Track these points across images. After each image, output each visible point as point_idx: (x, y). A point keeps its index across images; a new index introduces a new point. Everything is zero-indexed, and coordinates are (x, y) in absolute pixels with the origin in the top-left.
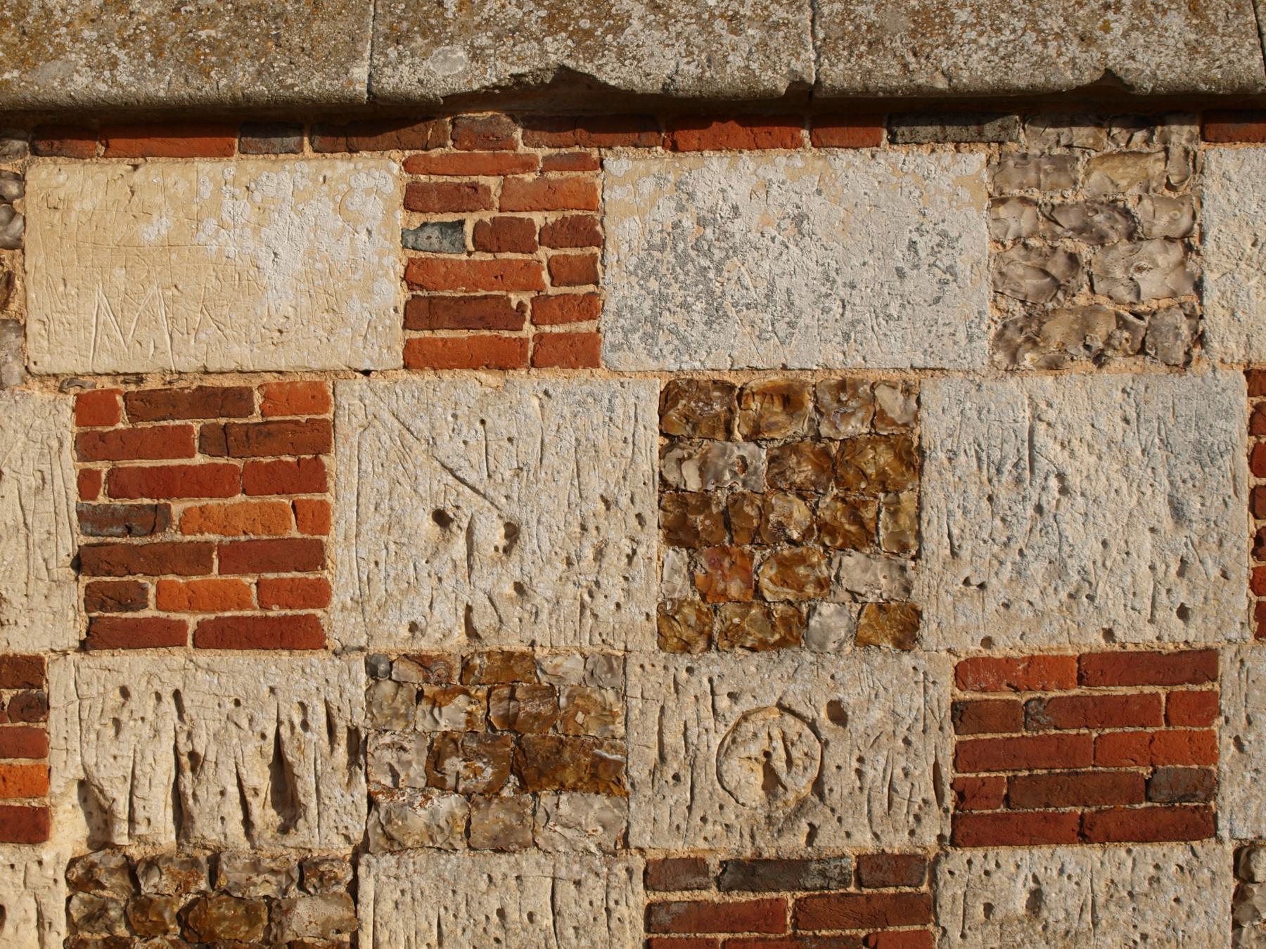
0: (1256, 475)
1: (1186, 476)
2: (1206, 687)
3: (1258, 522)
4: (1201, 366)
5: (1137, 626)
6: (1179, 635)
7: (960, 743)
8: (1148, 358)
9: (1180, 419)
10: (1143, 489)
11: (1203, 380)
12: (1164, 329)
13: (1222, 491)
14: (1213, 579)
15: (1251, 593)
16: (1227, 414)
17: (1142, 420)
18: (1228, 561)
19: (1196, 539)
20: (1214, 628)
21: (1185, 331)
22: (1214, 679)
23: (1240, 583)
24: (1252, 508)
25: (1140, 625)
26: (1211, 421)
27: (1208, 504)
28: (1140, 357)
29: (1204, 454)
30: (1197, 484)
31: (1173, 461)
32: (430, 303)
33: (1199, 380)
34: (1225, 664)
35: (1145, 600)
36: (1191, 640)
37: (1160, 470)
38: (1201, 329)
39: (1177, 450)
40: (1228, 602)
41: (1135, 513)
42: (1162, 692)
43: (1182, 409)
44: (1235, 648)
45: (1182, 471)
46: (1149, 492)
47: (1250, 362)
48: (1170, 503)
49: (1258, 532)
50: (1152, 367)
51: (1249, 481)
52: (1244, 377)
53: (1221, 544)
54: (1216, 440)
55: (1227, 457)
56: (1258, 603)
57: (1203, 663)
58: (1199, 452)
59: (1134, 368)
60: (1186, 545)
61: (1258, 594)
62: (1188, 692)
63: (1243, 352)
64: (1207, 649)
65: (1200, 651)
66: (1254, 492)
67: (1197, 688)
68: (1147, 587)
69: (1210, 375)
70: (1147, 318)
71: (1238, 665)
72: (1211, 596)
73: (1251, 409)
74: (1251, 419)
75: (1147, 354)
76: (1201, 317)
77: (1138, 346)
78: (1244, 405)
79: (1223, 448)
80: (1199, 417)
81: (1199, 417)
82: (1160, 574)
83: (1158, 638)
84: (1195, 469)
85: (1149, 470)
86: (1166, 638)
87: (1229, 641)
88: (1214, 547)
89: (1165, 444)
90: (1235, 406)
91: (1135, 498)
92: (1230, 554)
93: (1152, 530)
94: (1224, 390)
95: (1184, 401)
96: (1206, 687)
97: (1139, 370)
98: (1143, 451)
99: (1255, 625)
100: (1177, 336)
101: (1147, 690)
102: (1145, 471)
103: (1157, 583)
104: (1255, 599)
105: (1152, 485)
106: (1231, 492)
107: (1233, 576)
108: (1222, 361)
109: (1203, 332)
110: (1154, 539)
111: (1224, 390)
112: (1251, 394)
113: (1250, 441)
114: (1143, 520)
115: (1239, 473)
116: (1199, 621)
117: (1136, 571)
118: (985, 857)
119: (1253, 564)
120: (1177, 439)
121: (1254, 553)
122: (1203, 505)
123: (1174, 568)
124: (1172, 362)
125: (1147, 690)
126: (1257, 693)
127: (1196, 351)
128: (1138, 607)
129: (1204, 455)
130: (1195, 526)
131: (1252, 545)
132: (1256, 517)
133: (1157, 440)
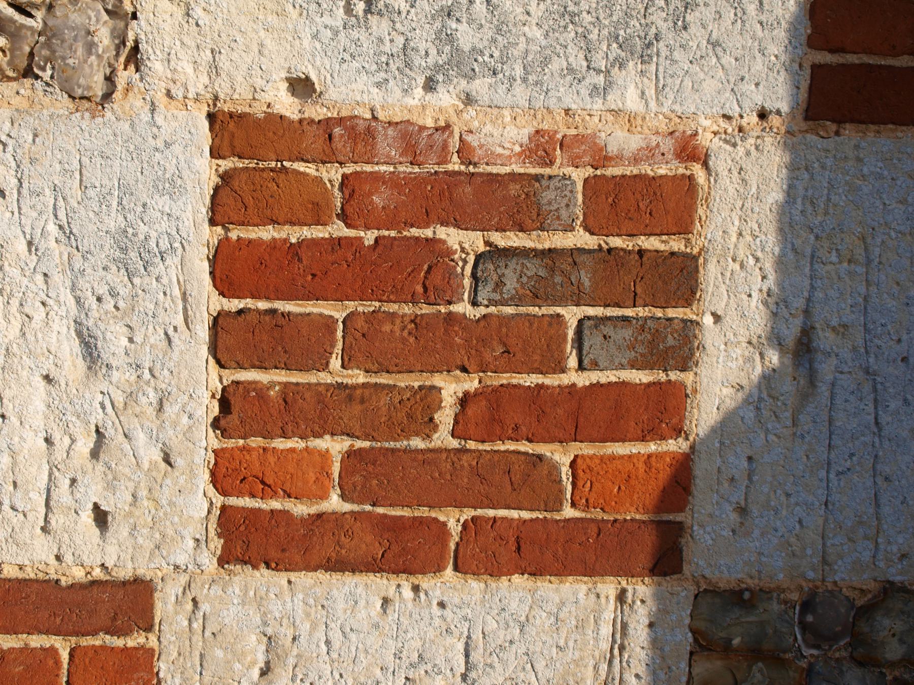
0: (222, 294)
1: (102, 290)
2: (135, 640)
3: (225, 373)
4: (129, 104)
5: (20, 538)
6: (87, 556)
7: (681, 510)
8: (39, 84)
9: (91, 193)
10: (27, 310)
11: (132, 126)
12: (68, 35)
13: (162, 317)
14: (146, 466)
15: (211, 491)
16: (171, 187)
17: (25, 191)
18: (171, 436)
19: (119, 398)
20: (149, 545)
21: (104, 38)
22: (149, 628)
23: (192, 474)
24: (214, 349)
25: (24, 536)
26: (144, 198)
27: (138, 339)
28: (28, 82)
29: (133, 255)
30: (121, 304)
31: (78, 264)
32: (318, 221)
33: (126, 126)
34: (166, 604)
35: (33, 495)
36: (110, 564)
37: (56, 278)
38: (131, 36)
39: (85, 245)
40: (171, 504)
41: (15, 349)
42: (63, 647)
43: (94, 176)
44: (183, 579)
45: (94, 281)
46: (39, 314)
47: (216, 98)
48: (79, 334)
49: (224, 389)
50: (47, 100)
51: (209, 301)
52: (206, 124)
53: (160, 408)
54: (154, 230)
55: (173, 261)
56: (224, 508)
57: (130, 601)
58: (124, 250)
59: (16, 101)
60: (103, 407)
61: (224, 493)
62: (103, 647)
63: (206, 80)
64: (137, 581)
65: (124, 583)
66: (218, 322)
67: (118, 642)
68: (37, 476)
69: (146, 117)
70: (39, 15)
71: (189, 606)
72: (143, 493)
73: (216, 180)
74: (214, 197)
75: (37, 77)
76: (134, 16)
77: (23, 64)
78: (204, 172)
79: (164, 244)
80: (125, 190)
81: (125, 190)
82: (59, 454)
83: (58, 558)
84: (117, 278)
85: (39, 278)
86: (68, 558)
87: (177, 567)
88: (151, 411)
89: (67, 233)
90: (186, 173)
91: (16, 325)
92: (175, 425)
93: (47, 378)
94: (167, 145)
95: (99, 160)
96: (135, 640)
97: (25, 104)
98: (30, 244)
99: (217, 544)
100: (90, 47)
101: (37, 641)
102: (32, 280)
103: (53, 468)
104: (219, 500)
105: (44, 304)
106: (179, 320)
107: (179, 462)
108: (169, 94)
109: (137, 42)
110: (49, 394)
111: (167, 145)
112: (215, 153)
113: (211, 235)
114: (27, 361)
115: (193, 291)
116: (125, 532)
117: (16, 448)
118: (621, 597)
119: (215, 443)
120: (86, 225)
121: (216, 424)
122: (131, 340)
123: (85, 445)
124: (79, 92)
125: (37, 641)
126: (219, 653)
127: (124, 76)
128: (20, 506)
129: (133, 255)
130: (116, 376)
131: (216, 410)
132: (221, 366)
133: (52, 228)
